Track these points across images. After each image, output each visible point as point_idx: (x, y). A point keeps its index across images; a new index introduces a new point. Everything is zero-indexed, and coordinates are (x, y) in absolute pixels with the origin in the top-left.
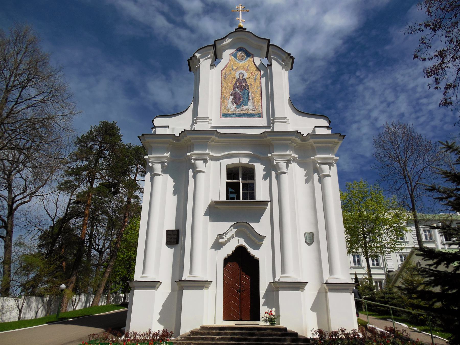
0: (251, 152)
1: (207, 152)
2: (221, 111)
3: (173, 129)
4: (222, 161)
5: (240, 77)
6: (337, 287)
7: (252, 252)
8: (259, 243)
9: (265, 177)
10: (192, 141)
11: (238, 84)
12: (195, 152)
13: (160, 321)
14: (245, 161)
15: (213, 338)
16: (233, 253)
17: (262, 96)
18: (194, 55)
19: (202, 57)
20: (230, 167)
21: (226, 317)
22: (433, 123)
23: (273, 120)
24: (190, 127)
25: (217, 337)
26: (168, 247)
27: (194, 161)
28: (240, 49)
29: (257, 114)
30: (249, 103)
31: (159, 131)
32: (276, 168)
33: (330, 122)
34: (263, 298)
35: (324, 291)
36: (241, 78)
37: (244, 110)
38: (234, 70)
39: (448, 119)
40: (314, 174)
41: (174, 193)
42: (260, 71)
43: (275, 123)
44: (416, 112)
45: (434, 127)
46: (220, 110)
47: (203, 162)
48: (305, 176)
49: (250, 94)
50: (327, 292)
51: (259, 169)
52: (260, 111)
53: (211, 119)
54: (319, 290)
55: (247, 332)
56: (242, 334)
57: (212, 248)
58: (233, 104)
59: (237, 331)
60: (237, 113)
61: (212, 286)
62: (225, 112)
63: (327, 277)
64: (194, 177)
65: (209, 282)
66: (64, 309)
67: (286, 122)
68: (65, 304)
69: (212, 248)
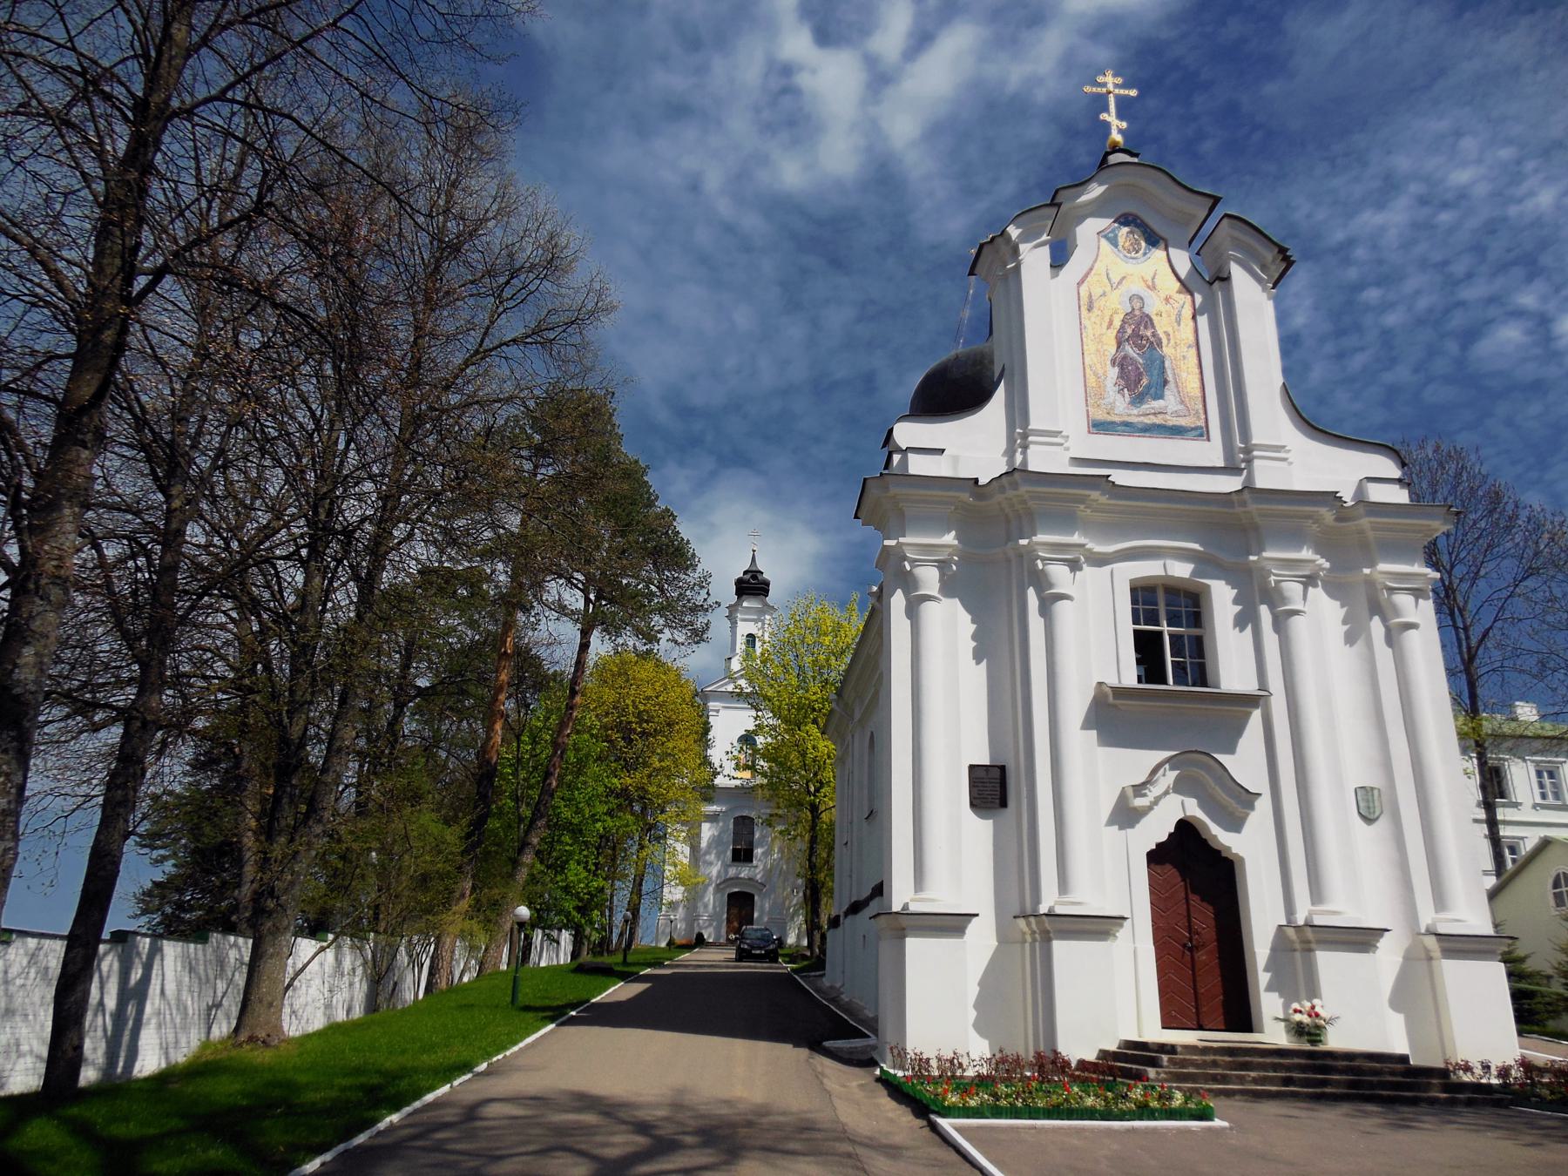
0: (1196, 546)
1: (1076, 538)
3: (956, 459)
4: (1115, 566)
6: (1482, 947)
8: (1240, 810)
9: (1241, 622)
11: (1129, 331)
12: (1041, 538)
14: (1181, 570)
15: (1243, 1076)
17: (1201, 373)
18: (1004, 231)
19: (1025, 238)
20: (1139, 584)
21: (1167, 1025)
23: (1248, 450)
24: (1003, 455)
27: (1044, 565)
28: (1125, 220)
29: (1193, 429)
30: (1167, 392)
31: (918, 466)
32: (1273, 597)
35: (1423, 955)
37: (1155, 414)
40: (1371, 619)
41: (978, 656)
42: (1192, 295)
43: (1257, 463)
46: (1084, 409)
47: (1067, 568)
48: (1345, 622)
49: (1167, 364)
50: (1430, 959)
51: (1222, 598)
56: (1205, 1064)
57: (1110, 822)
58: (1121, 391)
59: (1296, 1061)
61: (1123, 933)
62: (1100, 415)
64: (1045, 610)
67: (1284, 460)
69: (1110, 822)
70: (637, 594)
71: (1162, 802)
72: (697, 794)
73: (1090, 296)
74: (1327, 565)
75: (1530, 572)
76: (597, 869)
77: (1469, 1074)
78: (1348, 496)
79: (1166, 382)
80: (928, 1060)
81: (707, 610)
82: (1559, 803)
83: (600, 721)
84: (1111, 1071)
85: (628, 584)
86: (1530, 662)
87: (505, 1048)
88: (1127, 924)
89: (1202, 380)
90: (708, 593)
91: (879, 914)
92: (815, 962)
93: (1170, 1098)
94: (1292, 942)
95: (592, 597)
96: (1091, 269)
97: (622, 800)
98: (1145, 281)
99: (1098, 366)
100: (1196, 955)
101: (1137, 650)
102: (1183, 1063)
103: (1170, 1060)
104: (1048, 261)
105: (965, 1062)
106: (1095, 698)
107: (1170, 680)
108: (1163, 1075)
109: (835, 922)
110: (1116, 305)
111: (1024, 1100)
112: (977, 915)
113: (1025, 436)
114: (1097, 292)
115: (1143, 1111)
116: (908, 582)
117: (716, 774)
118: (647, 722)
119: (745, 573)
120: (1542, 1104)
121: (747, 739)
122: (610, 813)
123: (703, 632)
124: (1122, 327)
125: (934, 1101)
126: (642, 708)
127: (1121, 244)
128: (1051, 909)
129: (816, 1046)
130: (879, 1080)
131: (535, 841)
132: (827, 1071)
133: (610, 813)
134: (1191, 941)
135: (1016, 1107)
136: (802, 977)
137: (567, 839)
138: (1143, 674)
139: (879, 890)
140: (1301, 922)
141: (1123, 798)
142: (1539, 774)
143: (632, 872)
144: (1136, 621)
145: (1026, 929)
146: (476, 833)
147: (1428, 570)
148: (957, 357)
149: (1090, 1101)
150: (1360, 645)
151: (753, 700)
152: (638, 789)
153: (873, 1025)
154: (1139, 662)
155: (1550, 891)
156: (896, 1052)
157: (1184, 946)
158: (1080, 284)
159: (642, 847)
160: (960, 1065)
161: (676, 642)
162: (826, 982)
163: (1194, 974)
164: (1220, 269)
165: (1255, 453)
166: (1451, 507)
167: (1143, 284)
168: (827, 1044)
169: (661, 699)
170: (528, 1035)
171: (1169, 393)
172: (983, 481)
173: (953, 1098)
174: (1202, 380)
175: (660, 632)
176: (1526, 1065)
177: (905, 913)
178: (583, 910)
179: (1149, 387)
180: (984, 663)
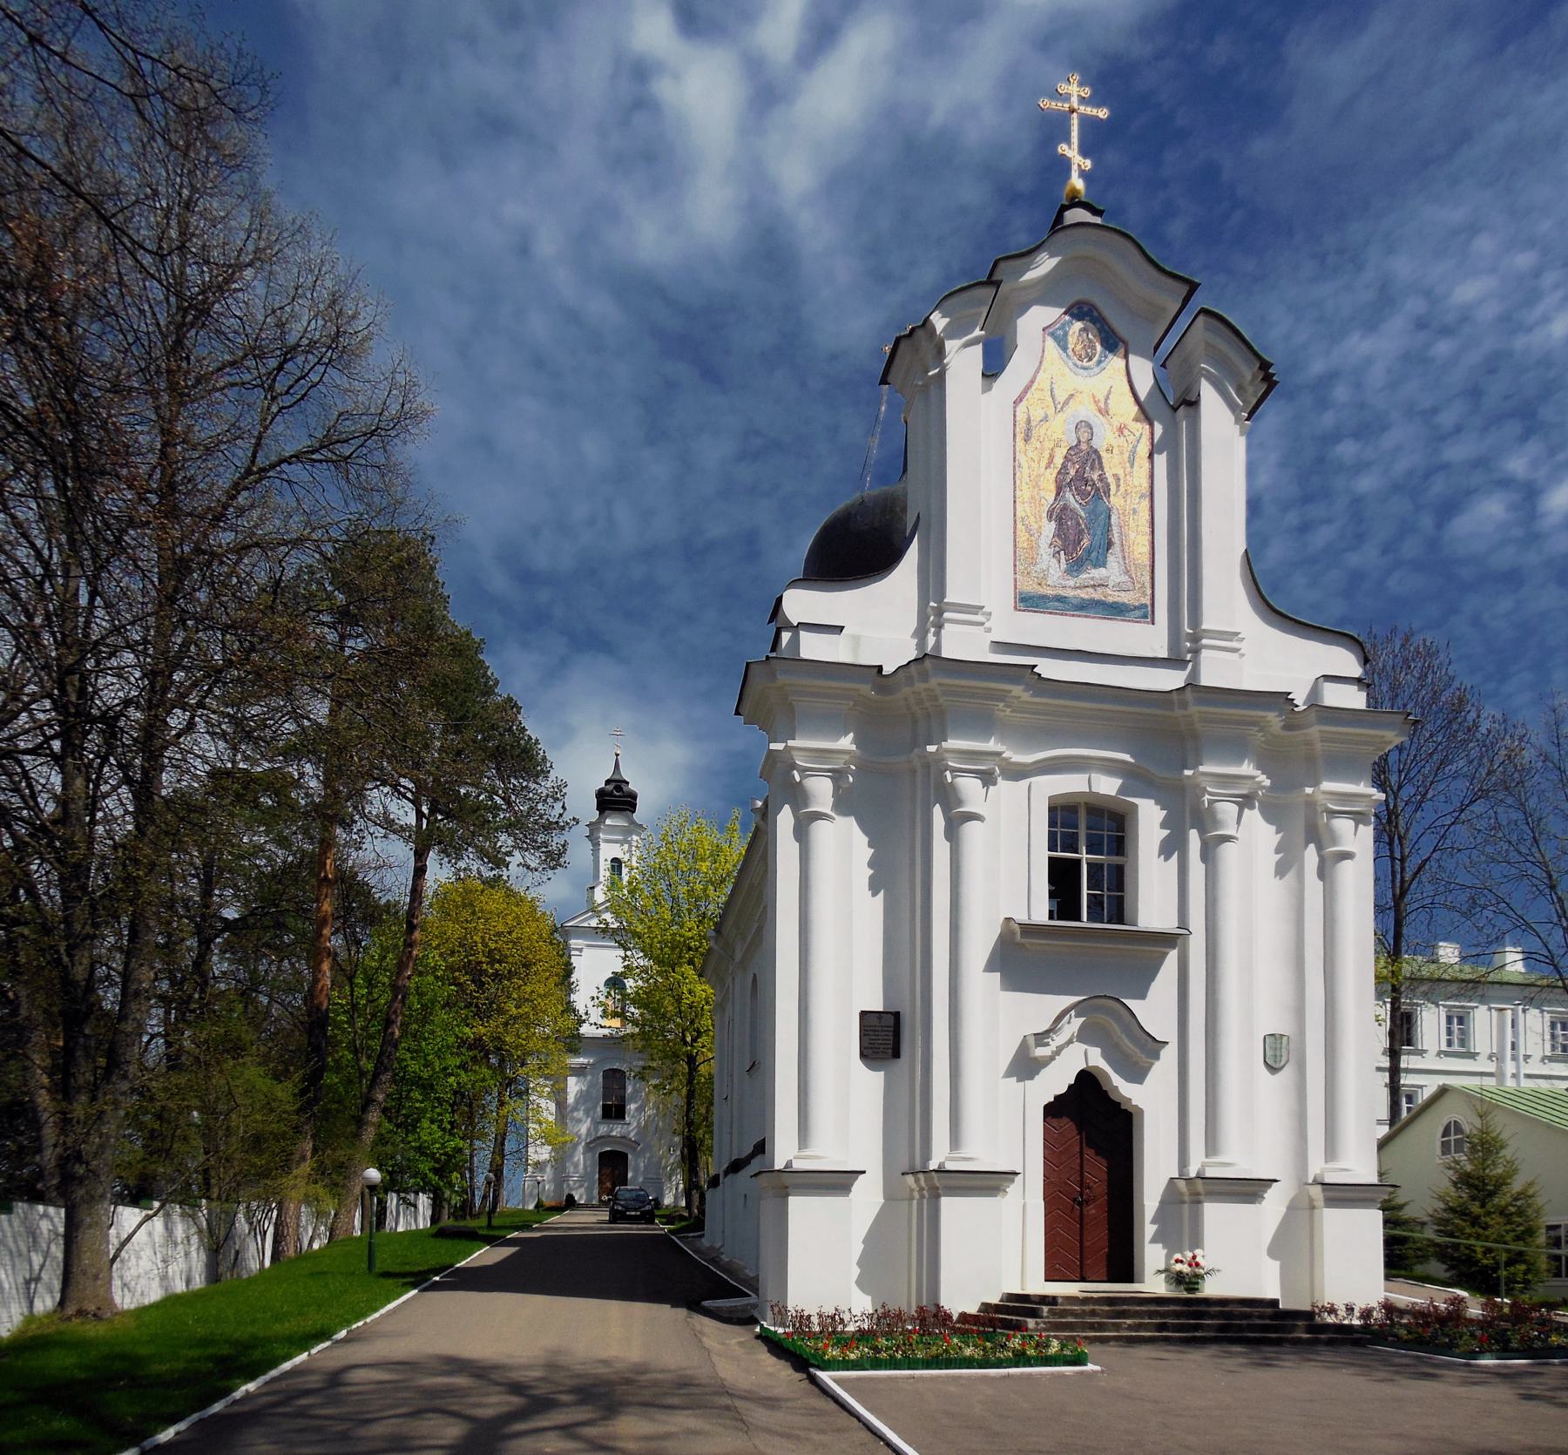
0: (1127, 757)
1: (992, 745)
2: (1015, 580)
4: (1033, 779)
7: (1124, 1088)
9: (1166, 849)
10: (941, 700)
11: (1072, 472)
12: (953, 743)
13: (862, 1283)
14: (1107, 786)
17: (1153, 532)
20: (1060, 802)
21: (1049, 1278)
22: (1353, 560)
23: (1196, 638)
25: (1129, 1321)
28: (1080, 311)
30: (1110, 558)
31: (813, 648)
32: (1204, 819)
33: (1365, 661)
34: (1153, 1222)
36: (1084, 447)
38: (1059, 407)
39: (1411, 548)
40: (1306, 846)
41: (874, 886)
42: (1151, 425)
43: (1205, 653)
44: (1307, 499)
45: (1356, 578)
46: (1012, 576)
47: (979, 781)
48: (1277, 851)
49: (1114, 519)
50: (1313, 1208)
51: (1150, 819)
52: (1144, 594)
53: (990, 614)
54: (1292, 1200)
55: (1178, 1308)
57: (1008, 1074)
59: (1153, 1308)
60: (1070, 593)
61: (1014, 1189)
62: (1029, 587)
63: (1317, 1165)
64: (952, 834)
69: (1008, 1074)
70: (478, 807)
73: (1029, 421)
74: (1267, 783)
76: (453, 1128)
78: (1300, 699)
79: (1110, 544)
80: (809, 1316)
81: (563, 828)
82: (1464, 1050)
84: (992, 1322)
85: (467, 795)
86: (1463, 897)
87: (365, 1315)
88: (1018, 1179)
90: (563, 807)
91: (760, 1173)
93: (1048, 1346)
94: (1182, 1194)
95: (425, 809)
96: (1032, 382)
99: (1032, 519)
101: (1050, 882)
102: (1064, 1313)
103: (1050, 1311)
105: (846, 1317)
106: (1001, 936)
107: (1085, 917)
109: (714, 1182)
110: (1059, 433)
111: (904, 1352)
112: (864, 1172)
113: (939, 612)
114: (1037, 415)
116: (797, 796)
118: (500, 962)
119: (608, 782)
120: (1400, 1343)
121: (615, 982)
122: (463, 1066)
123: (560, 855)
124: (1064, 466)
126: (493, 946)
127: (1071, 346)
129: (694, 1306)
130: (758, 1337)
131: (380, 1097)
132: (706, 1330)
133: (463, 1066)
136: (679, 1238)
137: (416, 1095)
138: (1055, 909)
140: (1193, 1175)
141: (1024, 1047)
142: (1449, 1020)
143: (492, 1130)
145: (914, 1186)
147: (1374, 791)
149: (968, 1352)
150: (1290, 876)
151: (620, 937)
153: (754, 1285)
154: (1052, 895)
156: (776, 1309)
157: (1074, 1200)
158: (1017, 402)
159: (502, 1104)
160: (842, 1320)
161: (528, 867)
162: (705, 1242)
164: (1188, 390)
165: (1204, 641)
167: (1093, 407)
168: (706, 1303)
169: (514, 935)
172: (887, 670)
173: (833, 1352)
175: (509, 854)
177: (788, 1171)
179: (1089, 551)
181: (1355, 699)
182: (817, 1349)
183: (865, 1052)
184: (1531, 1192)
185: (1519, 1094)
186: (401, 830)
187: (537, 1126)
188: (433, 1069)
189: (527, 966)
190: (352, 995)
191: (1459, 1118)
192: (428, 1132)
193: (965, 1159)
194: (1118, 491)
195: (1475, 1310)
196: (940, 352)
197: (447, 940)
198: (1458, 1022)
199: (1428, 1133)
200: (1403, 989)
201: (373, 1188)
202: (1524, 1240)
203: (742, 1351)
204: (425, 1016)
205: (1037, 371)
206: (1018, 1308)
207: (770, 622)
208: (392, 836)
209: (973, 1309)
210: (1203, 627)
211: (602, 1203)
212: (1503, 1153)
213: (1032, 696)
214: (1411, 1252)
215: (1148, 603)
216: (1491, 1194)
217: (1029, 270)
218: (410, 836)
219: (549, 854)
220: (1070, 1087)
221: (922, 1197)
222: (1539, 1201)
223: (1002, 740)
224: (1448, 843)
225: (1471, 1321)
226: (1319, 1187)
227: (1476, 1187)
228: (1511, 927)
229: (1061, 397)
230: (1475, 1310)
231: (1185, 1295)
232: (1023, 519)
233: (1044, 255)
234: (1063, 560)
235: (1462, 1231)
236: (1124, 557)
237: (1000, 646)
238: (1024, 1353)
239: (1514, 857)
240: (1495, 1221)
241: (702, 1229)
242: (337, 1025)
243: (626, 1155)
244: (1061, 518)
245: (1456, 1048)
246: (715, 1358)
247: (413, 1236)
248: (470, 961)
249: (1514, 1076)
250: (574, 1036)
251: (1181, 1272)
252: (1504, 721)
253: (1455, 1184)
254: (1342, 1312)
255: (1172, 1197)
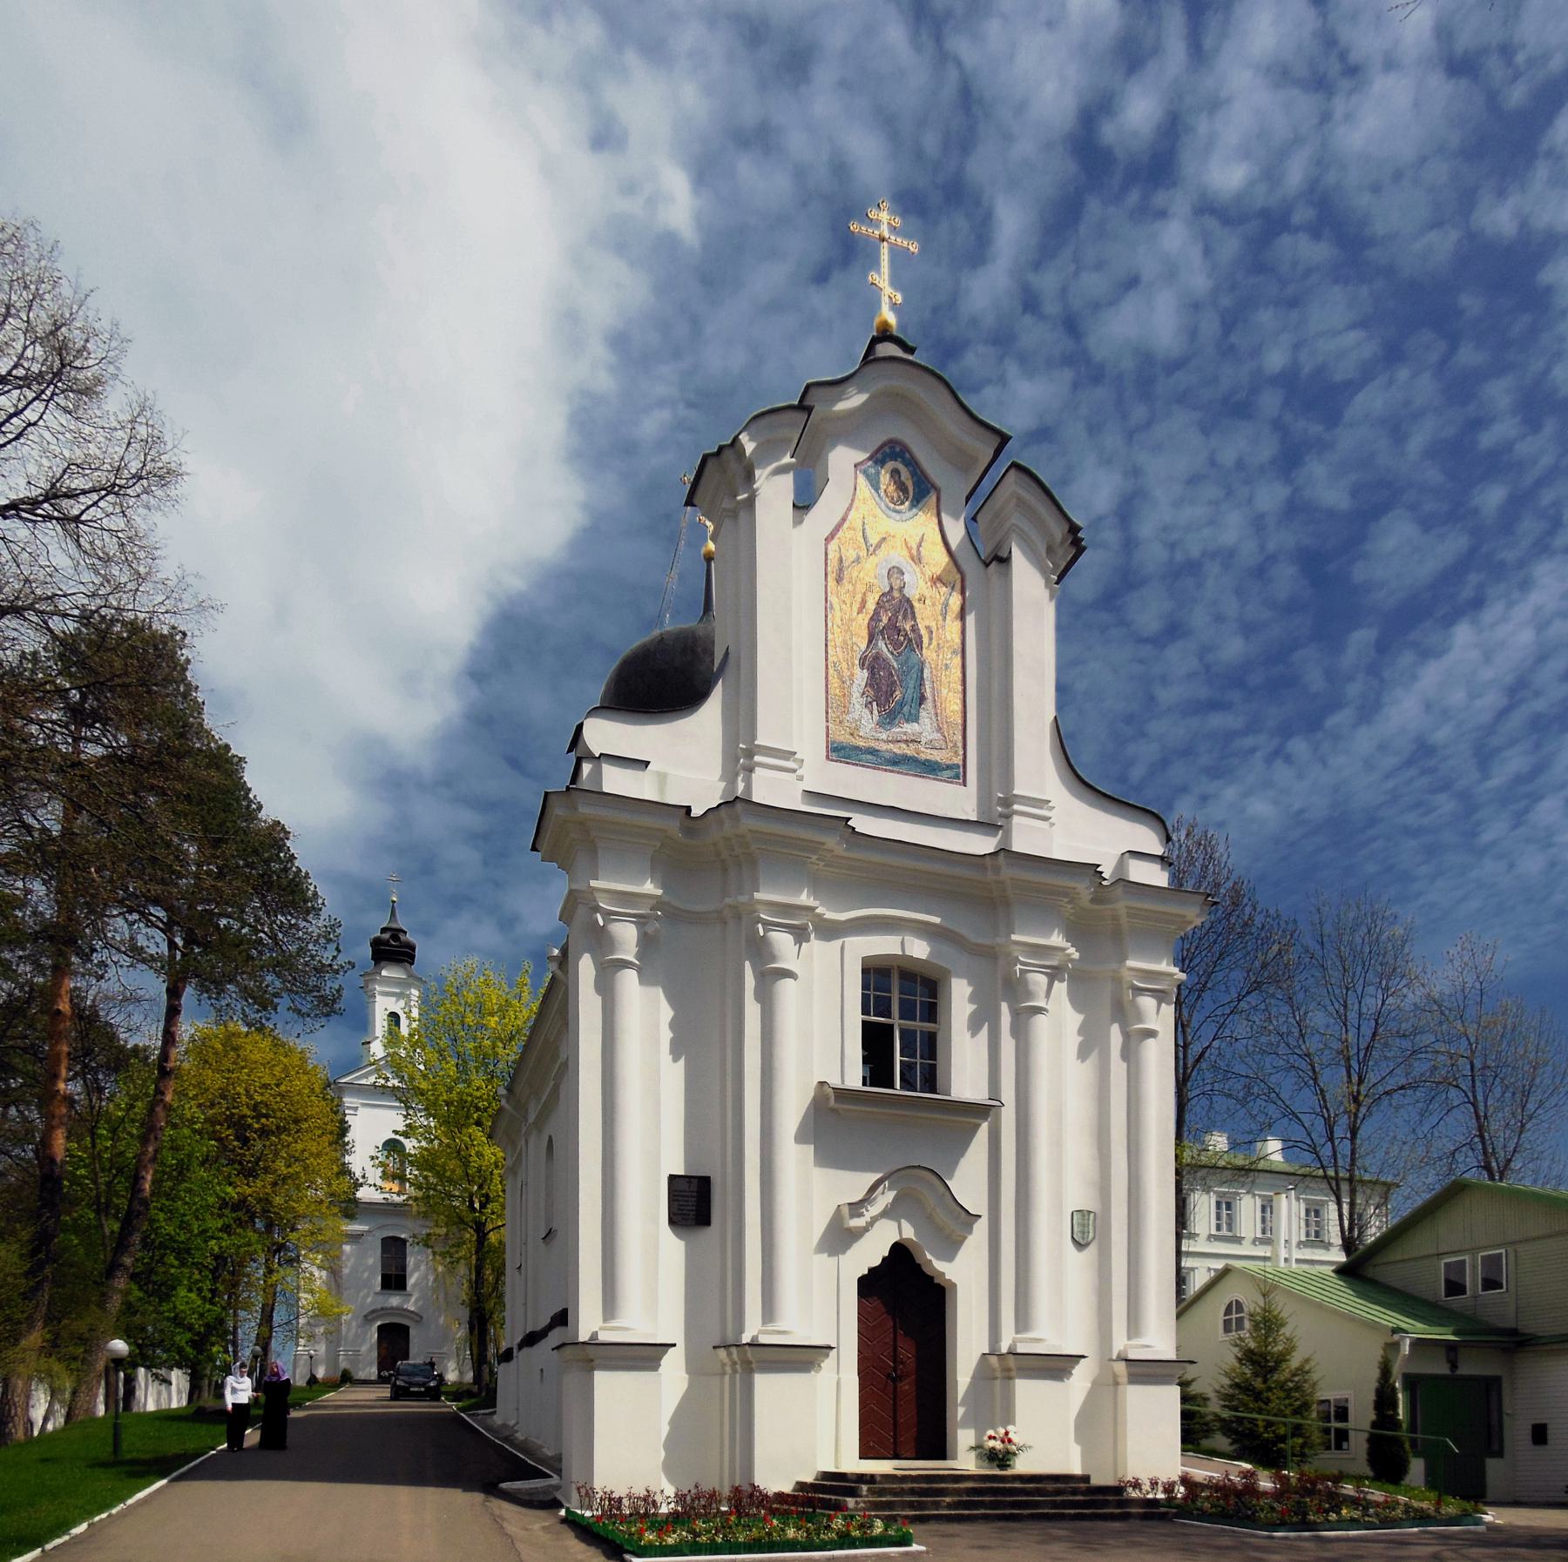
0: (937, 920)
2: (827, 727)
5: (892, 588)
9: (974, 1025)
11: (885, 620)
14: (919, 949)
15: (939, 1502)
16: (919, 1265)
18: (736, 439)
21: (865, 1454)
23: (1008, 801)
26: (677, 1236)
29: (948, 767)
30: (923, 714)
31: (615, 781)
32: (1015, 989)
35: (1111, 1381)
36: (896, 594)
37: (906, 742)
38: (871, 549)
41: (677, 1050)
43: (1016, 819)
46: (824, 724)
47: (790, 937)
50: (1116, 1384)
58: (868, 705)
60: (884, 747)
61: (828, 1364)
62: (842, 737)
63: (1120, 1342)
65: (824, 1350)
66: (22, 1428)
67: (1046, 819)
68: (19, 1410)
70: (240, 942)
71: (877, 1225)
72: (336, 1210)
73: (841, 560)
74: (1076, 955)
75: (1257, 986)
76: (213, 1297)
77: (1137, 1491)
78: (1107, 871)
79: (922, 699)
80: (620, 1499)
81: (337, 972)
82: (1230, 1234)
83: (204, 1113)
84: (810, 1502)
85: (228, 928)
86: (1237, 1086)
87: (111, 1506)
88: (833, 1353)
89: (965, 706)
90: (338, 950)
91: (563, 1345)
92: (482, 1393)
93: (871, 1527)
94: (994, 1370)
95: (179, 941)
96: (844, 520)
97: (240, 1214)
98: (909, 549)
99: (844, 665)
100: (899, 1385)
101: (864, 1048)
102: (881, 1492)
103: (869, 1490)
104: (790, 498)
105: (658, 1498)
106: (814, 1098)
107: (898, 1085)
108: (862, 1505)
109: (507, 1356)
110: (871, 575)
111: (725, 1536)
112: (674, 1345)
113: (750, 754)
114: (850, 554)
115: (845, 1541)
116: (600, 941)
117: (357, 1185)
118: (267, 1116)
120: (1203, 1516)
121: (392, 1146)
122: (226, 1229)
123: (334, 1001)
124: (876, 613)
125: (629, 1541)
126: (258, 1098)
127: (883, 487)
128: (755, 1338)
129: (490, 1488)
130: (564, 1521)
131: (128, 1261)
132: (506, 1515)
133: (226, 1229)
134: (895, 1371)
135: (716, 1543)
136: (469, 1416)
137: (171, 1259)
138: (868, 1075)
139: (562, 1319)
140: (1004, 1350)
141: (837, 1218)
142: (1218, 1204)
143: (258, 1300)
144: (865, 1011)
145: (726, 1360)
146: (41, 1249)
147: (1176, 970)
148: (661, 640)
149: (791, 1533)
150: (1093, 1058)
151: (403, 1097)
152: (260, 1201)
153: (557, 1464)
154: (865, 1061)
155: (1221, 1317)
156: (583, 1491)
157: (889, 1376)
158: (828, 540)
159: (270, 1271)
160: (654, 1502)
161: (299, 1012)
162: (498, 1420)
163: (895, 1404)
164: (999, 546)
165: (1016, 807)
166: (1209, 895)
167: (905, 552)
168: (504, 1485)
169: (283, 1088)
170: (140, 1491)
171: (926, 714)
172: (697, 812)
173: (650, 1536)
174: (965, 706)
175: (276, 995)
176: (1185, 1480)
177: (593, 1343)
178: (200, 1343)
179: (902, 704)
180: (682, 1062)
181: (1157, 877)
182: (631, 1534)
183: (674, 1219)
184: (1307, 1368)
185: (1293, 1275)
186: (149, 961)
187: (309, 1297)
188: (191, 1231)
189: (296, 1121)
190: (94, 1146)
191: (1241, 1298)
192: (186, 1299)
193: (779, 1332)
194: (930, 644)
195: (1266, 1483)
196: (749, 477)
197: (207, 1090)
198: (1226, 1206)
199: (1212, 1313)
200: (1184, 1173)
201: (118, 1362)
202: (1301, 1414)
203: (548, 1536)
204: (182, 1170)
205: (849, 509)
206: (835, 1486)
207: (570, 751)
208: (141, 966)
209: (787, 1488)
210: (1015, 792)
211: (382, 1380)
212: (1282, 1331)
213: (846, 849)
214: (1197, 1426)
215: (961, 763)
216: (1273, 1370)
217: (841, 400)
218: (162, 967)
219: (322, 999)
220: (884, 1259)
221: (735, 1371)
222: (1315, 1377)
223: (815, 893)
224: (1227, 1032)
225: (1265, 1493)
226: (1124, 1363)
227: (1259, 1363)
228: (1280, 1116)
229: (874, 540)
230: (1266, 1483)
231: (997, 1472)
232: (835, 663)
233: (851, 390)
234: (875, 712)
235: (1245, 1405)
236: (936, 714)
237: (811, 795)
238: (848, 1535)
239: (1282, 1050)
240: (1276, 1398)
241: (494, 1406)
242: (75, 1180)
243: (408, 1328)
244: (873, 668)
245: (1224, 1232)
246: (519, 1546)
247: (166, 1417)
248: (233, 1114)
249: (1286, 1260)
250: (350, 1201)
251: (994, 1448)
252: (1278, 916)
253: (1240, 1360)
254: (1146, 1487)
255: (984, 1372)
